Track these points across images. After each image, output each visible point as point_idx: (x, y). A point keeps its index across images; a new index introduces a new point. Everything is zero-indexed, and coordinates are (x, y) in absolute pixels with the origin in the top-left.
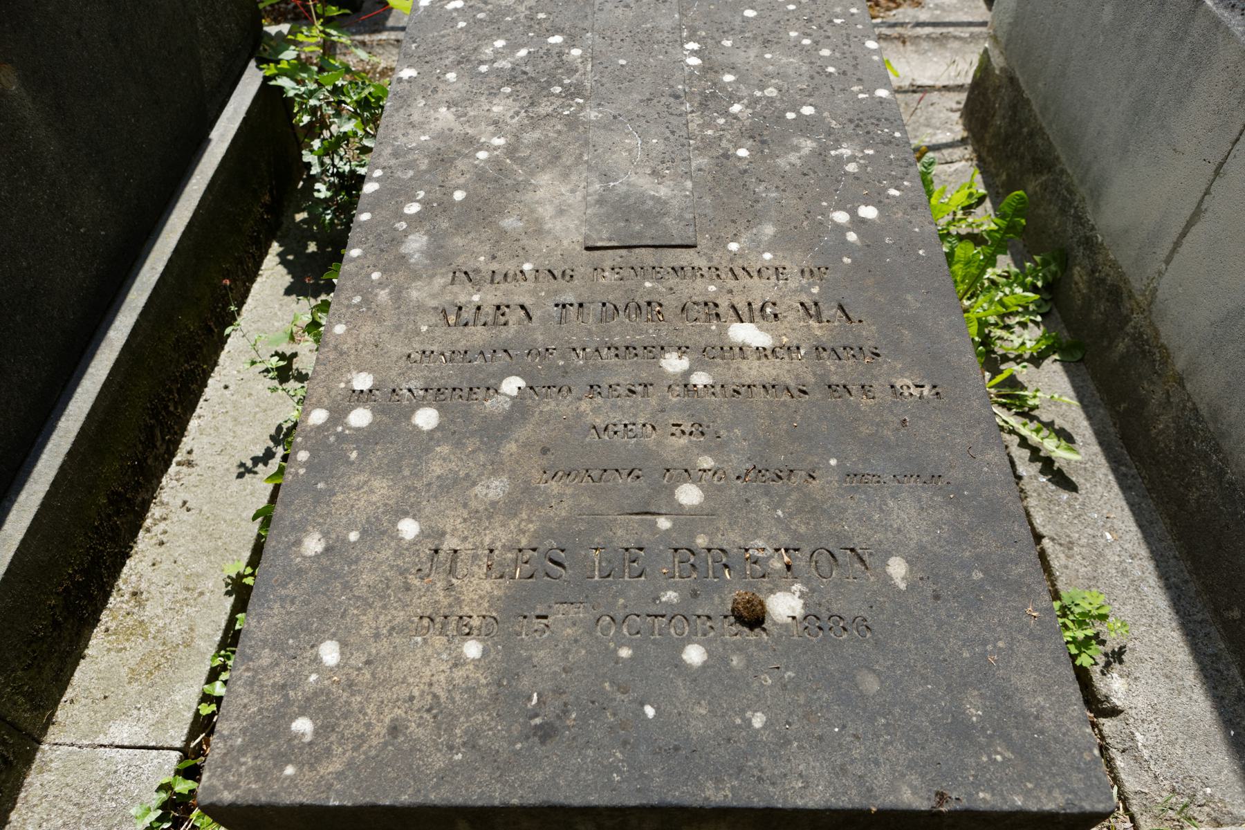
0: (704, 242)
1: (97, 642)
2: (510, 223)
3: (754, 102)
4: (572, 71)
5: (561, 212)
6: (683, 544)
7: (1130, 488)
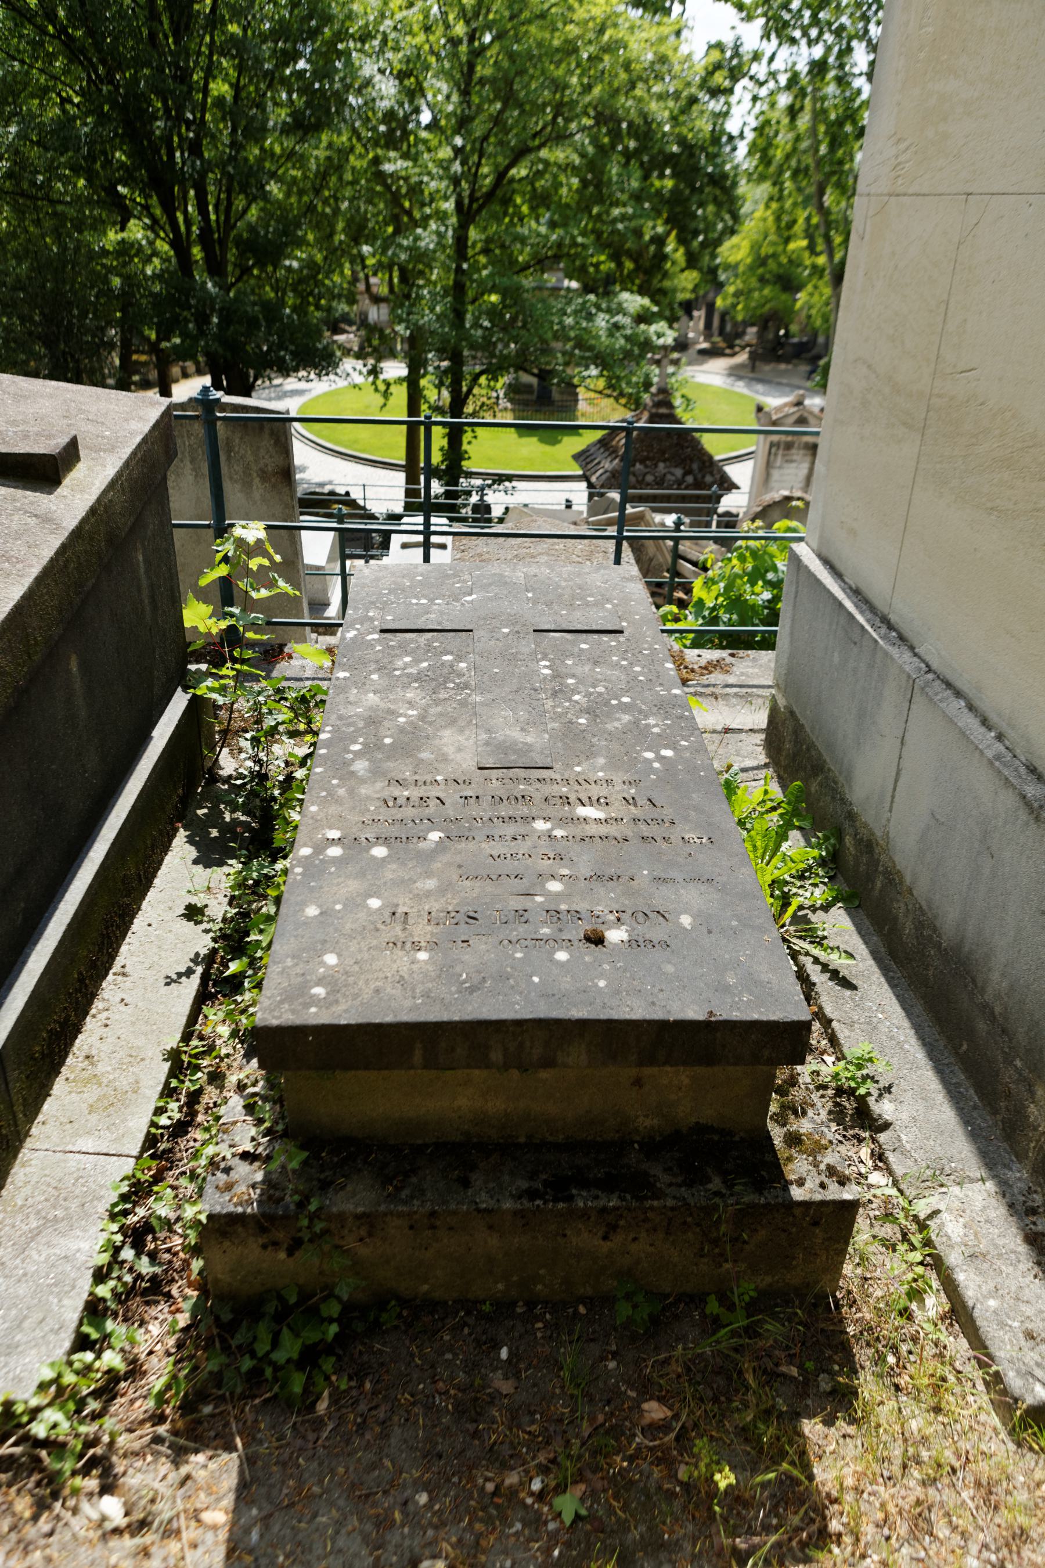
0: (557, 766)
1: (59, 1087)
2: (425, 755)
3: (588, 695)
4: (461, 675)
5: (459, 750)
6: (553, 907)
7: (897, 985)
